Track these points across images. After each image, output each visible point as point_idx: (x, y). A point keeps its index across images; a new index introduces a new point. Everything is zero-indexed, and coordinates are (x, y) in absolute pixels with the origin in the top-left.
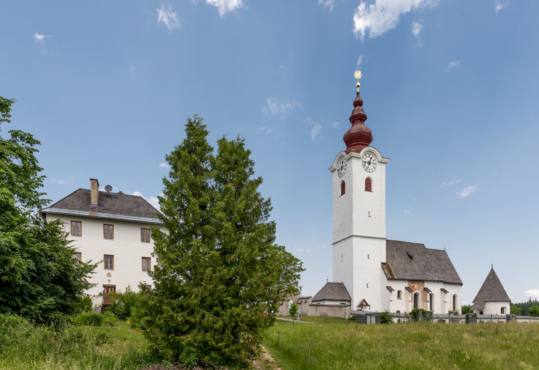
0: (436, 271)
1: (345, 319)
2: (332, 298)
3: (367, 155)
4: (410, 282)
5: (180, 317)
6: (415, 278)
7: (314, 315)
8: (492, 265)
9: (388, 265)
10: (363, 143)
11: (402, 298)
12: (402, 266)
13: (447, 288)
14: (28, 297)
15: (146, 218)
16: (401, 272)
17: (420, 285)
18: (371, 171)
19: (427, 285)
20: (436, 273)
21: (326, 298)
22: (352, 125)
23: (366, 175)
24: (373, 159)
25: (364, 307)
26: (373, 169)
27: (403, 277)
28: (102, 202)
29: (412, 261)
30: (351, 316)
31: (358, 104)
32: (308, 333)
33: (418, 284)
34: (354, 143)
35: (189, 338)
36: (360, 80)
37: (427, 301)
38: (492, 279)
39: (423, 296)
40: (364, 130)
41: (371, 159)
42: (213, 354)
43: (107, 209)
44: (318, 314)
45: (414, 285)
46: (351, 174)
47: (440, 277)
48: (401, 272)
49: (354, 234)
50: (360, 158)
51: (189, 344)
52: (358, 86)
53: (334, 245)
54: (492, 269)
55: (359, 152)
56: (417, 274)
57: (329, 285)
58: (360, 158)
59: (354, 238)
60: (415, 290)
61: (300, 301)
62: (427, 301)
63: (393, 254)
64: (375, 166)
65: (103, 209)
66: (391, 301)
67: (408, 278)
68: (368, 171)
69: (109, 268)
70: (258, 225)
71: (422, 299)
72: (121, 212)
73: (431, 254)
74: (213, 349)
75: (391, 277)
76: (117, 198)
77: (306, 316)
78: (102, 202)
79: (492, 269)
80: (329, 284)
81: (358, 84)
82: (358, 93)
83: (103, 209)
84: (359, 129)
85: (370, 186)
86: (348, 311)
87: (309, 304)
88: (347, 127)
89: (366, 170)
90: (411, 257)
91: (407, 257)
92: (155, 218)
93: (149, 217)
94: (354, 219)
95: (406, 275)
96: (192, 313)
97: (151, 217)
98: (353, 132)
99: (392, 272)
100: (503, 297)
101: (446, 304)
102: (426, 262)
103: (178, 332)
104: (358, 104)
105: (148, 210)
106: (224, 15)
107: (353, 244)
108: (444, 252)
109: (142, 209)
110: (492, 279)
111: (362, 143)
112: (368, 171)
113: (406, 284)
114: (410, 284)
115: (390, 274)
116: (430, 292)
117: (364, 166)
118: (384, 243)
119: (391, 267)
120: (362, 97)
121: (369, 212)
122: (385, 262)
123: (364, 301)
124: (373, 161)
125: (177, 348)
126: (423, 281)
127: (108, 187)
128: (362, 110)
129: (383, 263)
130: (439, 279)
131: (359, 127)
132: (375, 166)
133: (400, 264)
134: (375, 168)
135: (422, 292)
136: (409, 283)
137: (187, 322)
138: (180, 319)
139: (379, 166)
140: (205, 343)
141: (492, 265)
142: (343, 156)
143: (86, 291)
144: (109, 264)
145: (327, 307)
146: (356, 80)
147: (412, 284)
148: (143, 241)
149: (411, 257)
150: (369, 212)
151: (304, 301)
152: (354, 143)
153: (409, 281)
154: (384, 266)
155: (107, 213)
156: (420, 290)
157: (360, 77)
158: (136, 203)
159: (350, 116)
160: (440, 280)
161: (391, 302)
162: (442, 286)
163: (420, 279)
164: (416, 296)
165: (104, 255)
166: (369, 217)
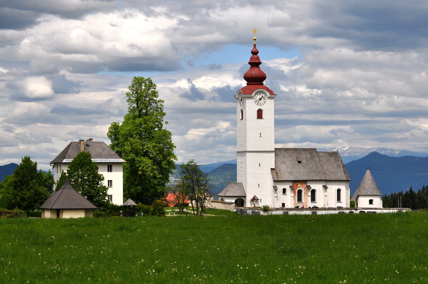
4: (293, 182)
11: (342, 201)
14: (27, 190)
18: (262, 104)
23: (258, 107)
26: (264, 103)
34: (251, 83)
45: (298, 184)
53: (239, 154)
55: (251, 94)
60: (299, 188)
69: (110, 171)
70: (141, 211)
89: (258, 104)
90: (300, 162)
104: (255, 53)
106: (169, 177)
121: (260, 134)
122: (274, 168)
123: (255, 196)
129: (272, 169)
134: (265, 102)
135: (305, 189)
139: (268, 101)
143: (163, 166)
147: (296, 183)
150: (260, 134)
152: (251, 83)
164: (300, 192)
165: (271, 168)
166: (261, 137)
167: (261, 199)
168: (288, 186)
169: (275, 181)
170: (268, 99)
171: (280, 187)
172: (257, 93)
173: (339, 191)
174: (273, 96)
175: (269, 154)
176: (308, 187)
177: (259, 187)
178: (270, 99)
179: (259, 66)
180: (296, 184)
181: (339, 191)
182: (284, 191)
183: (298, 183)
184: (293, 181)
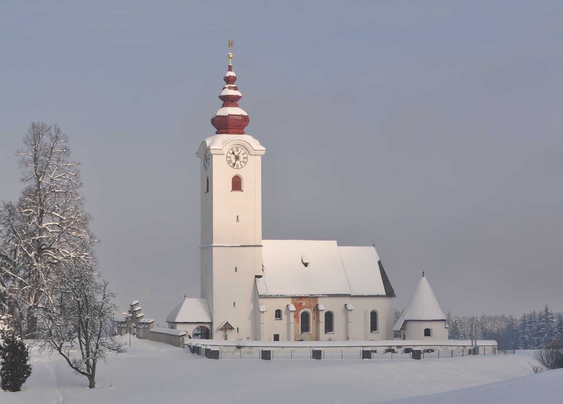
8: (423, 272)
18: (240, 167)
33: (308, 300)
45: (302, 302)
60: (303, 308)
101: (350, 313)
124: (243, 154)
134: (245, 163)
141: (423, 272)
175: (480, 354)
183: (303, 300)
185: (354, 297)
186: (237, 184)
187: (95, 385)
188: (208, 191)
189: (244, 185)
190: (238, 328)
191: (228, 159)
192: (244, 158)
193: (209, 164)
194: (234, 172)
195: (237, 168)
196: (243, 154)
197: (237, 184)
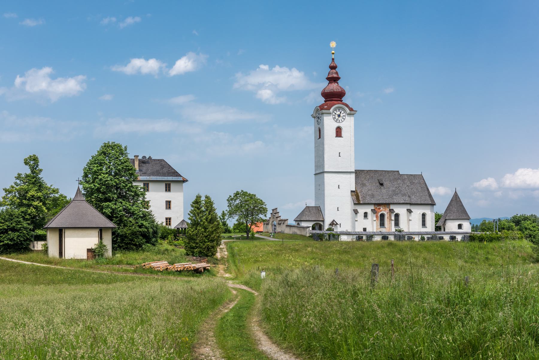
0: (404, 195)
1: (306, 236)
2: (308, 219)
3: (337, 110)
5: (194, 245)
6: (381, 202)
7: (288, 233)
9: (357, 193)
10: (336, 99)
12: (370, 193)
13: (413, 208)
15: (169, 177)
16: (368, 197)
17: (386, 208)
18: (341, 121)
19: (392, 207)
20: (403, 196)
21: (302, 220)
22: (329, 83)
24: (342, 112)
25: (334, 225)
26: (343, 120)
27: (369, 202)
28: (141, 168)
29: (382, 188)
30: (311, 234)
31: (333, 68)
32: (213, 247)
34: (328, 99)
35: (196, 250)
36: (335, 49)
37: (392, 220)
38: (456, 199)
39: (389, 216)
40: (335, 91)
41: (341, 113)
42: (202, 254)
43: (145, 173)
44: (291, 233)
45: (380, 207)
46: (323, 125)
47: (407, 199)
48: (368, 197)
49: (325, 170)
50: (330, 113)
51: (196, 251)
52: (333, 54)
54: (456, 192)
55: (329, 109)
56: (383, 199)
57: (308, 208)
58: (330, 113)
59: (326, 175)
60: (381, 211)
61: (280, 222)
62: (392, 220)
63: (365, 182)
64: (344, 117)
65: (142, 173)
66: (356, 221)
67: (374, 202)
68: (338, 122)
71: (388, 218)
72: (153, 174)
73: (403, 180)
74: (202, 252)
75: (357, 203)
76: (149, 163)
77: (284, 233)
78: (141, 168)
79: (456, 192)
80: (308, 208)
81: (333, 52)
82: (333, 59)
83: (142, 173)
84: (331, 90)
85: (341, 133)
86: (308, 231)
87: (286, 225)
88: (324, 85)
89: (336, 121)
91: (378, 184)
92: (174, 176)
93: (170, 176)
94: (326, 159)
95: (372, 200)
96: (197, 244)
97: (172, 176)
98: (326, 91)
99: (359, 198)
100: (463, 214)
101: (410, 222)
102: (396, 187)
103: (193, 248)
104: (333, 68)
105: (169, 170)
107: (325, 178)
108: (421, 177)
109: (165, 170)
110: (456, 199)
111: (334, 99)
112: (338, 122)
113: (373, 207)
114: (376, 207)
115: (357, 200)
116: (394, 213)
117: (334, 118)
118: (353, 176)
119: (359, 194)
120: (337, 62)
121: (339, 153)
122: (354, 190)
123: (334, 220)
124: (343, 114)
125: (193, 252)
126: (389, 204)
127: (144, 157)
128: (337, 73)
129: (352, 191)
130: (404, 202)
131: (334, 87)
132: (344, 117)
133: (369, 190)
134: (344, 119)
135: (388, 213)
136: (374, 206)
137: (196, 246)
138: (194, 246)
140: (200, 251)
142: (318, 109)
144: (168, 223)
145: (296, 228)
146: (332, 49)
148: (166, 190)
149: (382, 184)
150: (339, 153)
151: (283, 222)
152: (328, 99)
153: (375, 204)
154: (353, 194)
155: (145, 176)
156: (386, 211)
157: (334, 46)
158: (161, 165)
159: (327, 77)
160: (406, 202)
161: (356, 222)
162: (409, 207)
163: (385, 202)
164: (382, 216)
166: (340, 156)
167: (340, 224)
168: (370, 210)
169: (355, 204)
170: (347, 116)
171: (362, 210)
172: (335, 109)
173: (424, 215)
174: (352, 112)
175: (348, 176)
176: (391, 211)
177: (339, 188)
178: (349, 115)
179: (338, 82)
180: (378, 208)
181: (424, 215)
182: (366, 215)
184: (375, 204)
185: (347, 173)
186: (339, 132)
187: (482, 181)
188: (320, 137)
189: (343, 134)
190: (340, 224)
191: (334, 117)
192: (344, 116)
193: (320, 120)
194: (337, 125)
195: (339, 122)
196: (343, 114)
197: (339, 132)
